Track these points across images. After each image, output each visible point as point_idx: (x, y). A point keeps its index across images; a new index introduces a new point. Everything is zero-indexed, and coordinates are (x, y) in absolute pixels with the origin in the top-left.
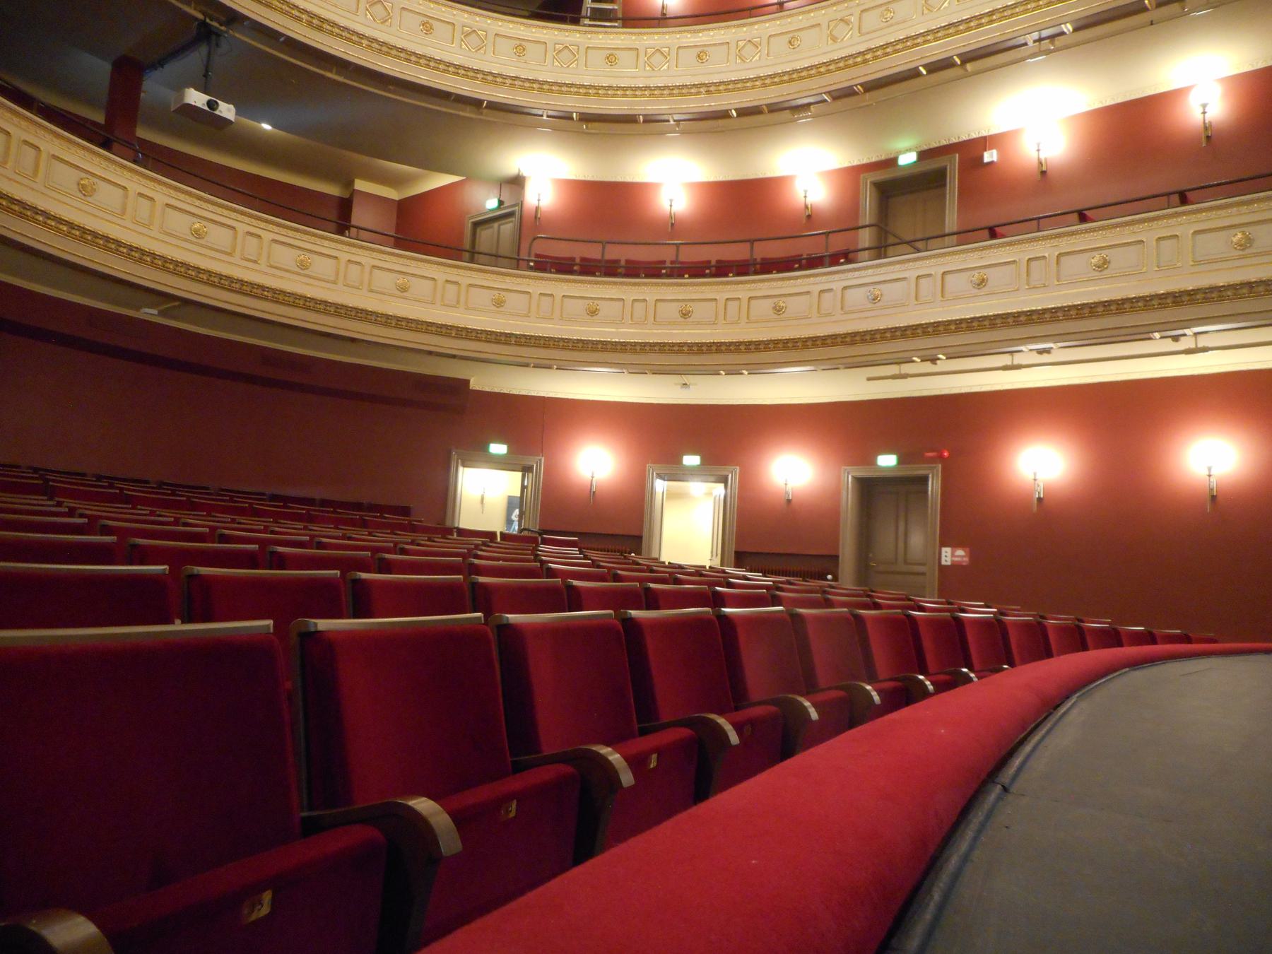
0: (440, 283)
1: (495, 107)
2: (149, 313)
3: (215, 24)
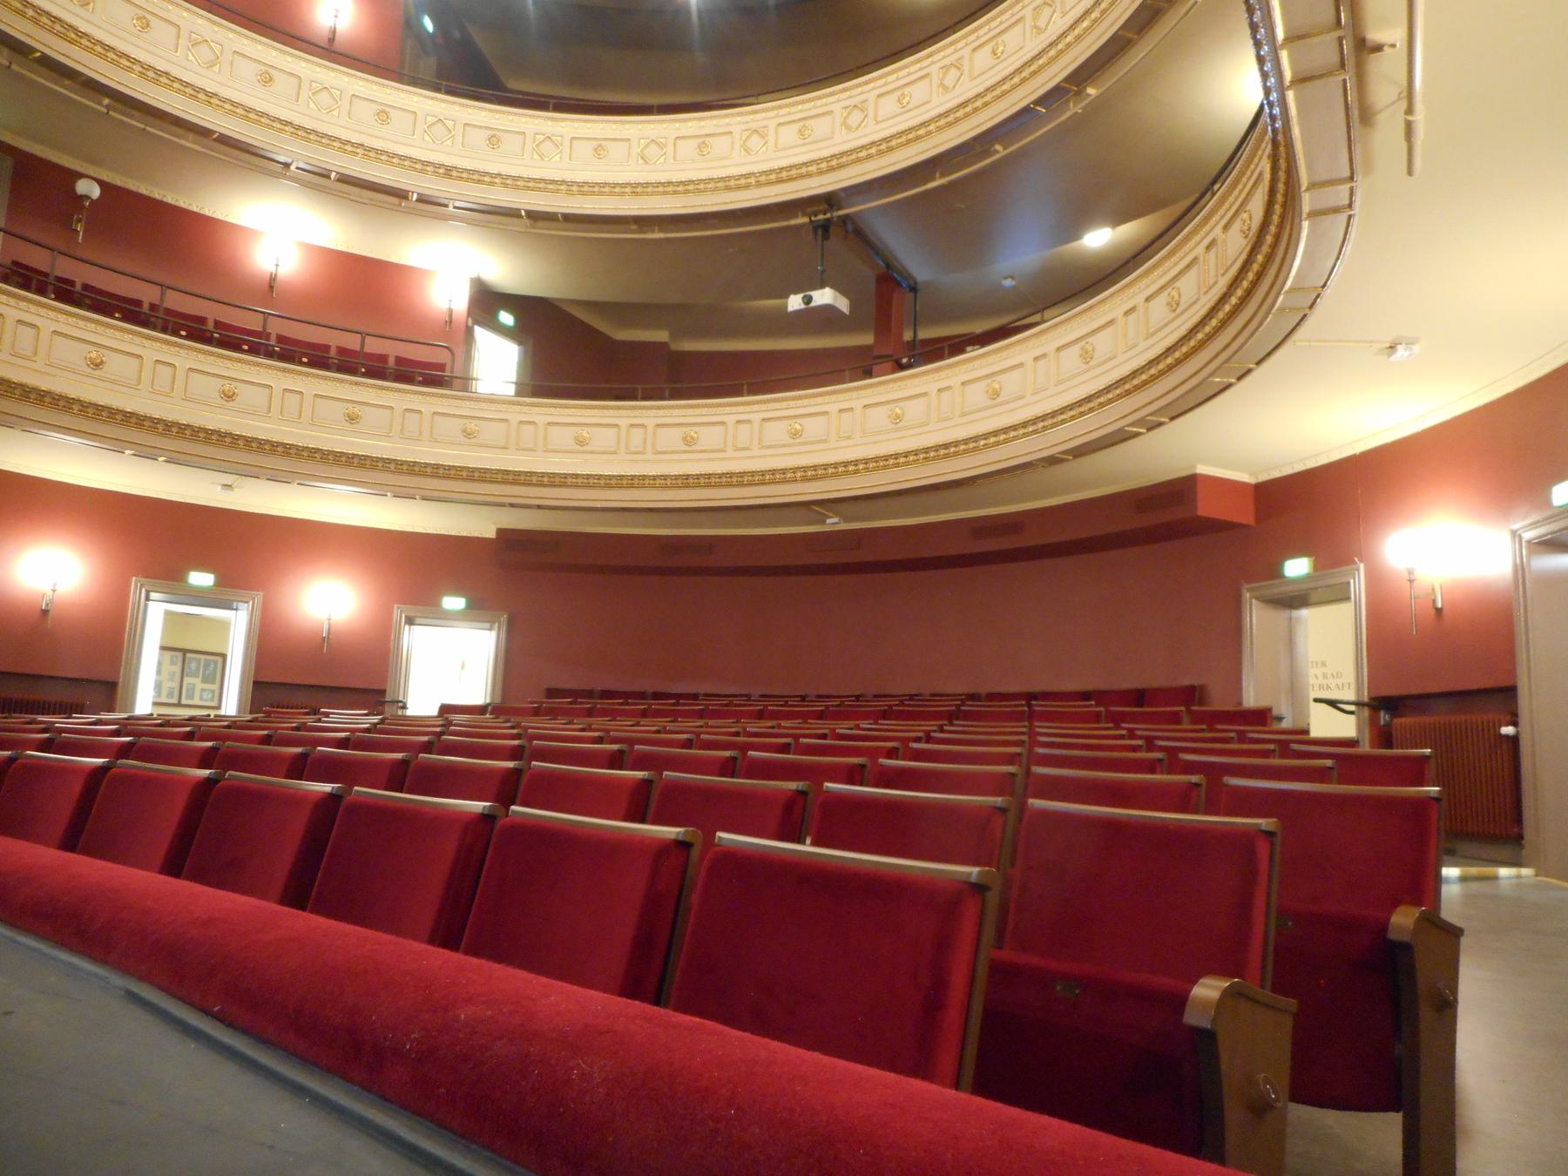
0: (277, 392)
2: (833, 523)
3: (821, 217)
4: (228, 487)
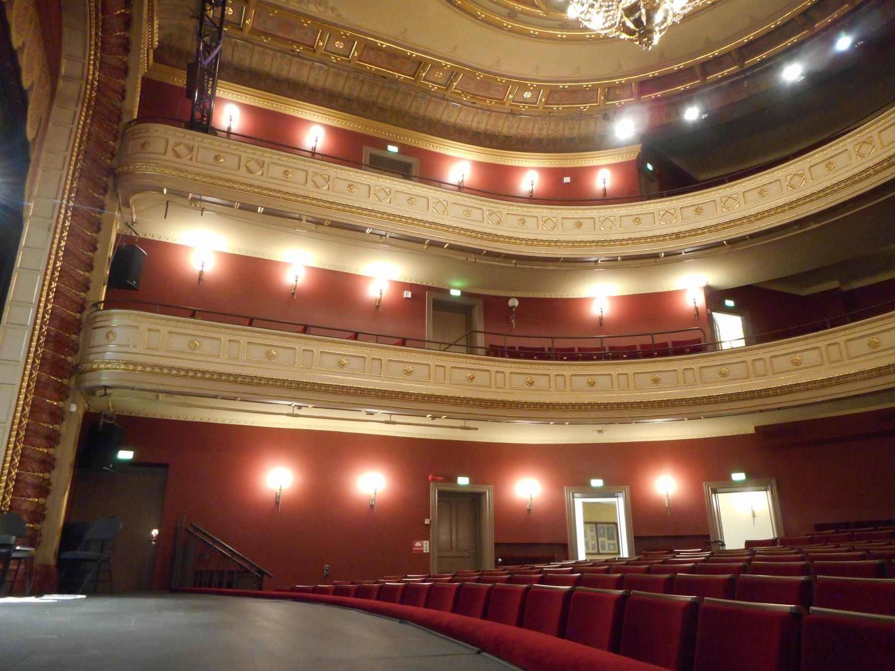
1: (567, 260)
4: (600, 431)
